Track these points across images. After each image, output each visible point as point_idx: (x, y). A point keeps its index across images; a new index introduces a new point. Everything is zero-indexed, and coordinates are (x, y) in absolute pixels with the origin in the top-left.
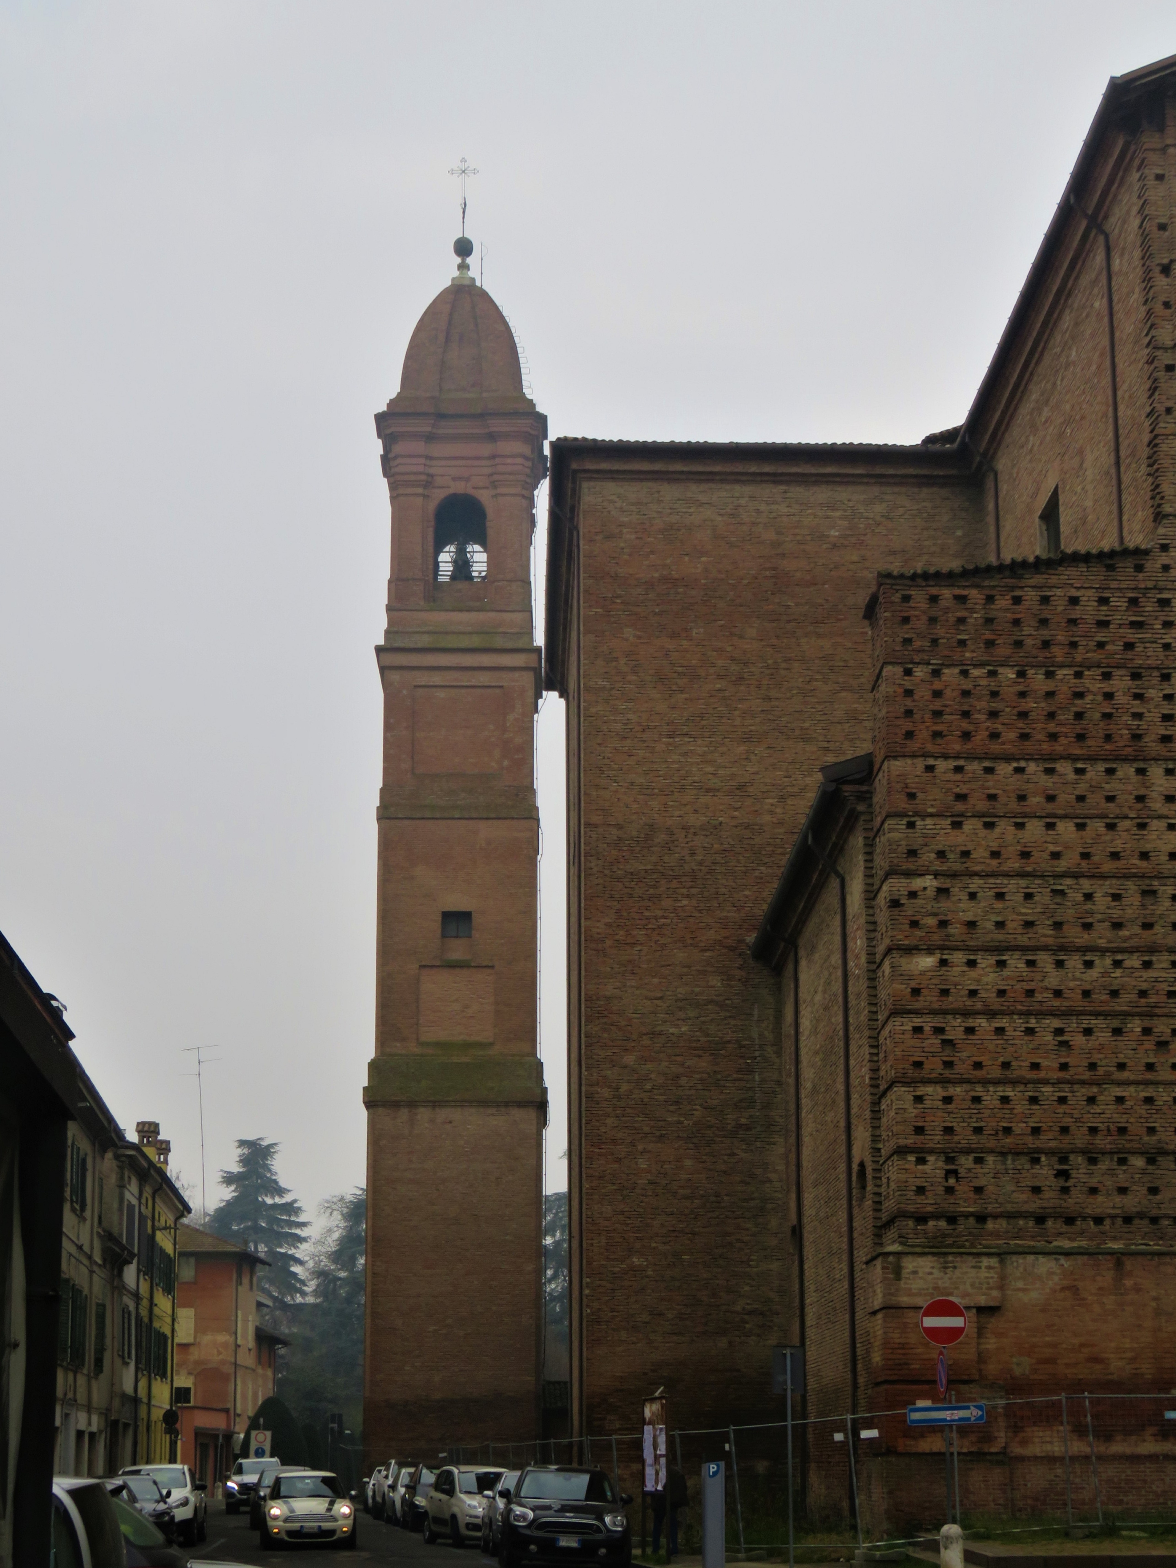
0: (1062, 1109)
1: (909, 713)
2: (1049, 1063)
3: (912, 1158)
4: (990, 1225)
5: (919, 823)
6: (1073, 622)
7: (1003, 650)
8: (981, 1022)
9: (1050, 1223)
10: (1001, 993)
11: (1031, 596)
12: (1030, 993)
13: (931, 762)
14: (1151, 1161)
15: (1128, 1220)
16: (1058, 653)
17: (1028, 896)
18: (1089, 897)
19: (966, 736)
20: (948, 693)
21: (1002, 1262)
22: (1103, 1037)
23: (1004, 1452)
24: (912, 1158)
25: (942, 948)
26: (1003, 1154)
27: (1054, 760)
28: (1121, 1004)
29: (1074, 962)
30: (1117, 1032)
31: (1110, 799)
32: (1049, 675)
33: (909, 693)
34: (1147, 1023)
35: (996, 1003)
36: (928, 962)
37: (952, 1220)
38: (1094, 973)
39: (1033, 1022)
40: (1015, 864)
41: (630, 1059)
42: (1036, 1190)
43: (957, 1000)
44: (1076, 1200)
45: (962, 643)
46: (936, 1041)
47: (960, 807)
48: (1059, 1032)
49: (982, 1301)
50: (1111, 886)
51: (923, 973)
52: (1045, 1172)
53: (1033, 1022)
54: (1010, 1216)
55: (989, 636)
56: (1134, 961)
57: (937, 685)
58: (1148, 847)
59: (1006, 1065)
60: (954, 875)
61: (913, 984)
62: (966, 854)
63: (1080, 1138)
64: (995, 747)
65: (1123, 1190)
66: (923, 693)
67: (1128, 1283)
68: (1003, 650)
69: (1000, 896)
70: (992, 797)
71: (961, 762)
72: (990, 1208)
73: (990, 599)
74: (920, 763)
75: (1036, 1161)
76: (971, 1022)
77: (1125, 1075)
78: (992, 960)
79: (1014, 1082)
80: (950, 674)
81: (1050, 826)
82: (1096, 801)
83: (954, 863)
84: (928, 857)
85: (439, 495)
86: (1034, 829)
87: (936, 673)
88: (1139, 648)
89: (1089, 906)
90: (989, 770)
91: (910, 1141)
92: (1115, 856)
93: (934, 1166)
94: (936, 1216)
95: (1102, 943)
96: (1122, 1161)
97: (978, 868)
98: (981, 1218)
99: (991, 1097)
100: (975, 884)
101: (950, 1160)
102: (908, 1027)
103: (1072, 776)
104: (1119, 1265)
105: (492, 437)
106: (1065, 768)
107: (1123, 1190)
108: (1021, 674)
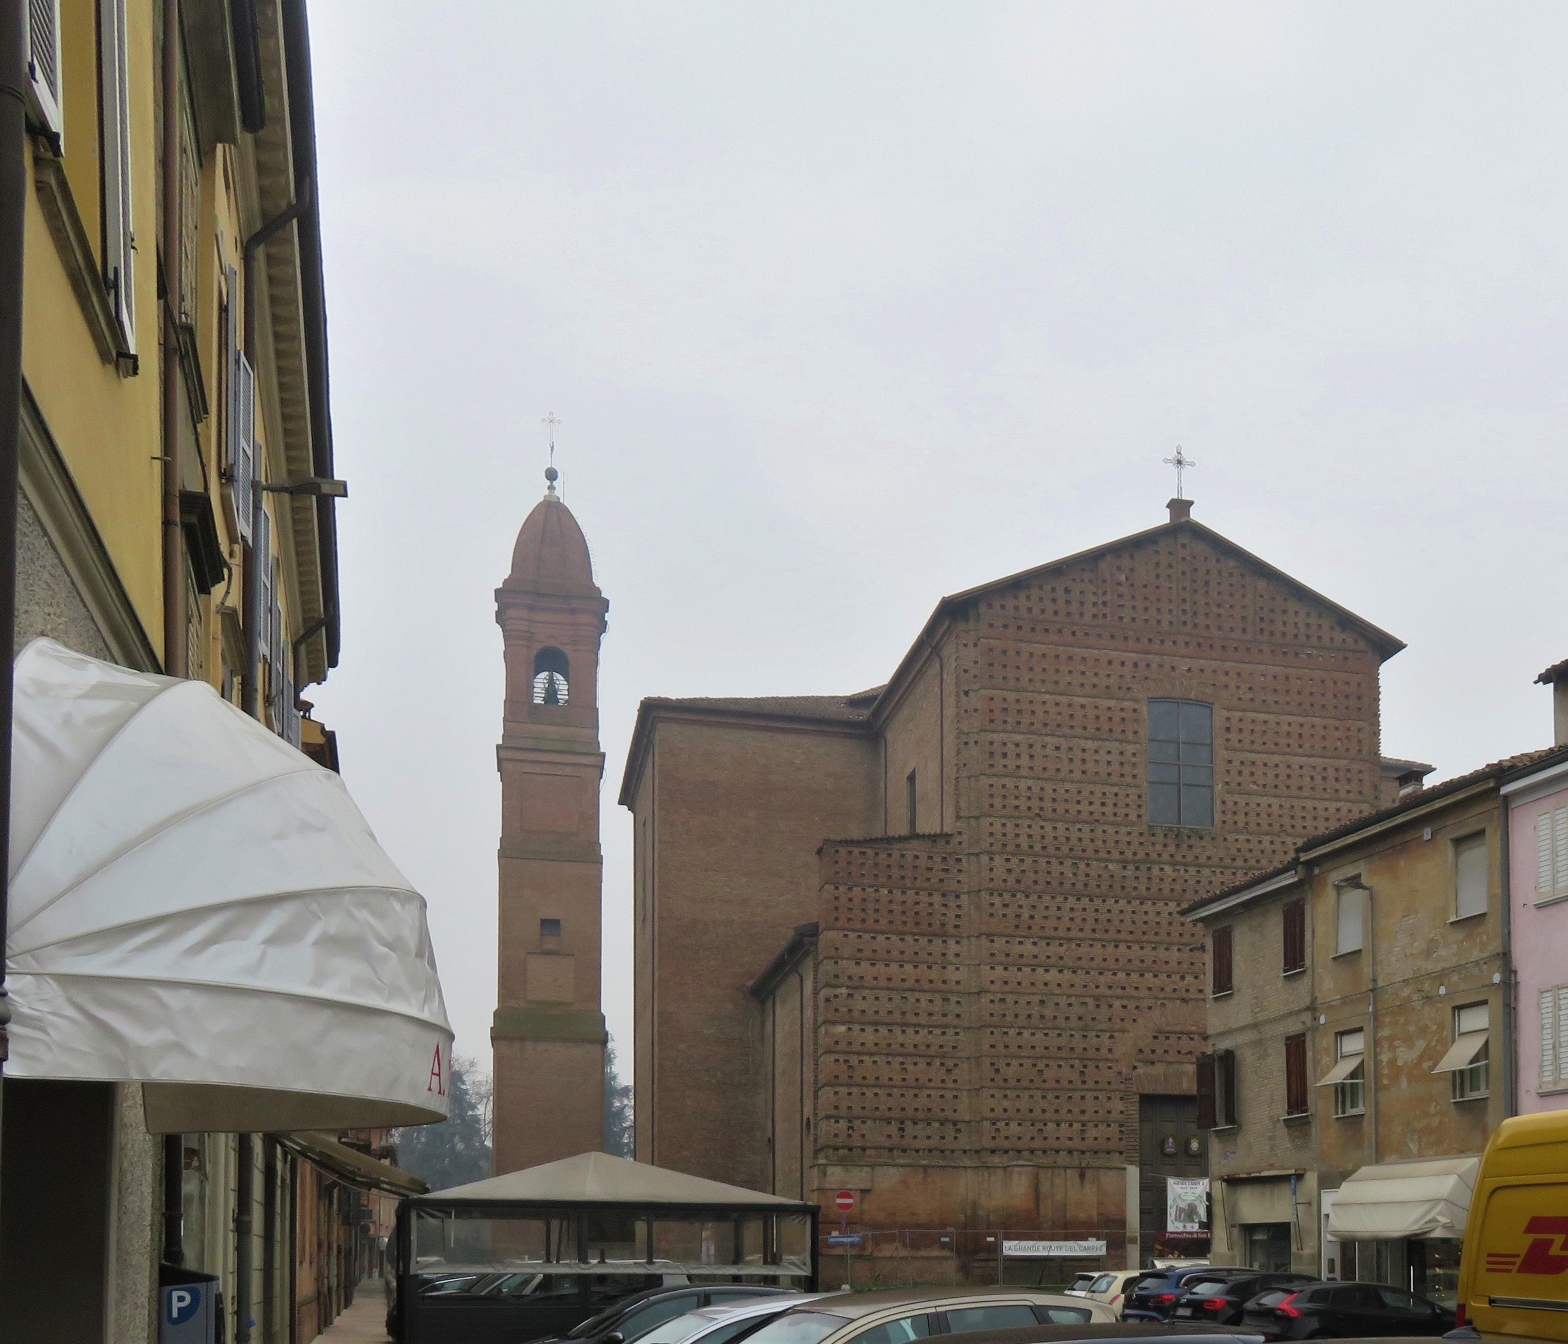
0: (902, 1099)
1: (836, 908)
2: (897, 1078)
3: (833, 1120)
4: (868, 1152)
5: (840, 962)
6: (915, 867)
7: (882, 880)
8: (866, 1058)
9: (895, 1151)
10: (876, 1044)
11: (896, 854)
12: (889, 1045)
13: (846, 932)
14: (942, 1124)
15: (930, 1151)
16: (908, 883)
17: (890, 999)
18: (918, 1000)
19: (863, 921)
20: (855, 899)
21: (872, 1169)
22: (922, 1066)
23: (871, 1255)
24: (833, 1120)
25: (849, 1022)
26: (875, 1120)
27: (904, 934)
28: (932, 1051)
29: (910, 1031)
30: (929, 1064)
31: (930, 954)
32: (904, 893)
33: (837, 898)
34: (942, 1061)
35: (874, 1049)
36: (842, 1029)
37: (850, 1149)
38: (919, 1037)
39: (890, 1059)
40: (883, 983)
41: (682, 1046)
42: (889, 1136)
43: (856, 1047)
44: (905, 1142)
45: (863, 875)
46: (844, 1067)
47: (859, 955)
48: (902, 1063)
49: (862, 1187)
50: (928, 996)
51: (840, 1033)
52: (893, 1128)
53: (890, 1059)
54: (876, 1148)
55: (876, 872)
56: (938, 1032)
57: (851, 895)
58: (946, 978)
59: (877, 1078)
60: (856, 988)
61: (835, 1039)
62: (862, 978)
63: (910, 1112)
64: (877, 927)
65: (928, 1137)
66: (843, 899)
67: (929, 1180)
68: (882, 880)
69: (877, 998)
70: (875, 951)
71: (861, 934)
72: (868, 1145)
73: (877, 854)
74: (841, 934)
75: (889, 1123)
76: (861, 1058)
77: (932, 1084)
78: (872, 1029)
79: (880, 1087)
80: (857, 890)
81: (902, 966)
82: (923, 955)
83: (856, 982)
84: (843, 979)
85: (538, 646)
86: (894, 967)
87: (850, 889)
88: (946, 881)
89: (918, 1005)
90: (874, 938)
91: (832, 1112)
92: (931, 981)
93: (843, 1124)
94: (843, 1147)
95: (923, 1022)
96: (929, 1124)
97: (866, 985)
98: (864, 1149)
99: (869, 1093)
100: (866, 992)
101: (850, 1121)
102: (833, 1059)
103: (912, 942)
104: (925, 1171)
105: (573, 611)
106: (909, 939)
107: (928, 1137)
108: (890, 892)
